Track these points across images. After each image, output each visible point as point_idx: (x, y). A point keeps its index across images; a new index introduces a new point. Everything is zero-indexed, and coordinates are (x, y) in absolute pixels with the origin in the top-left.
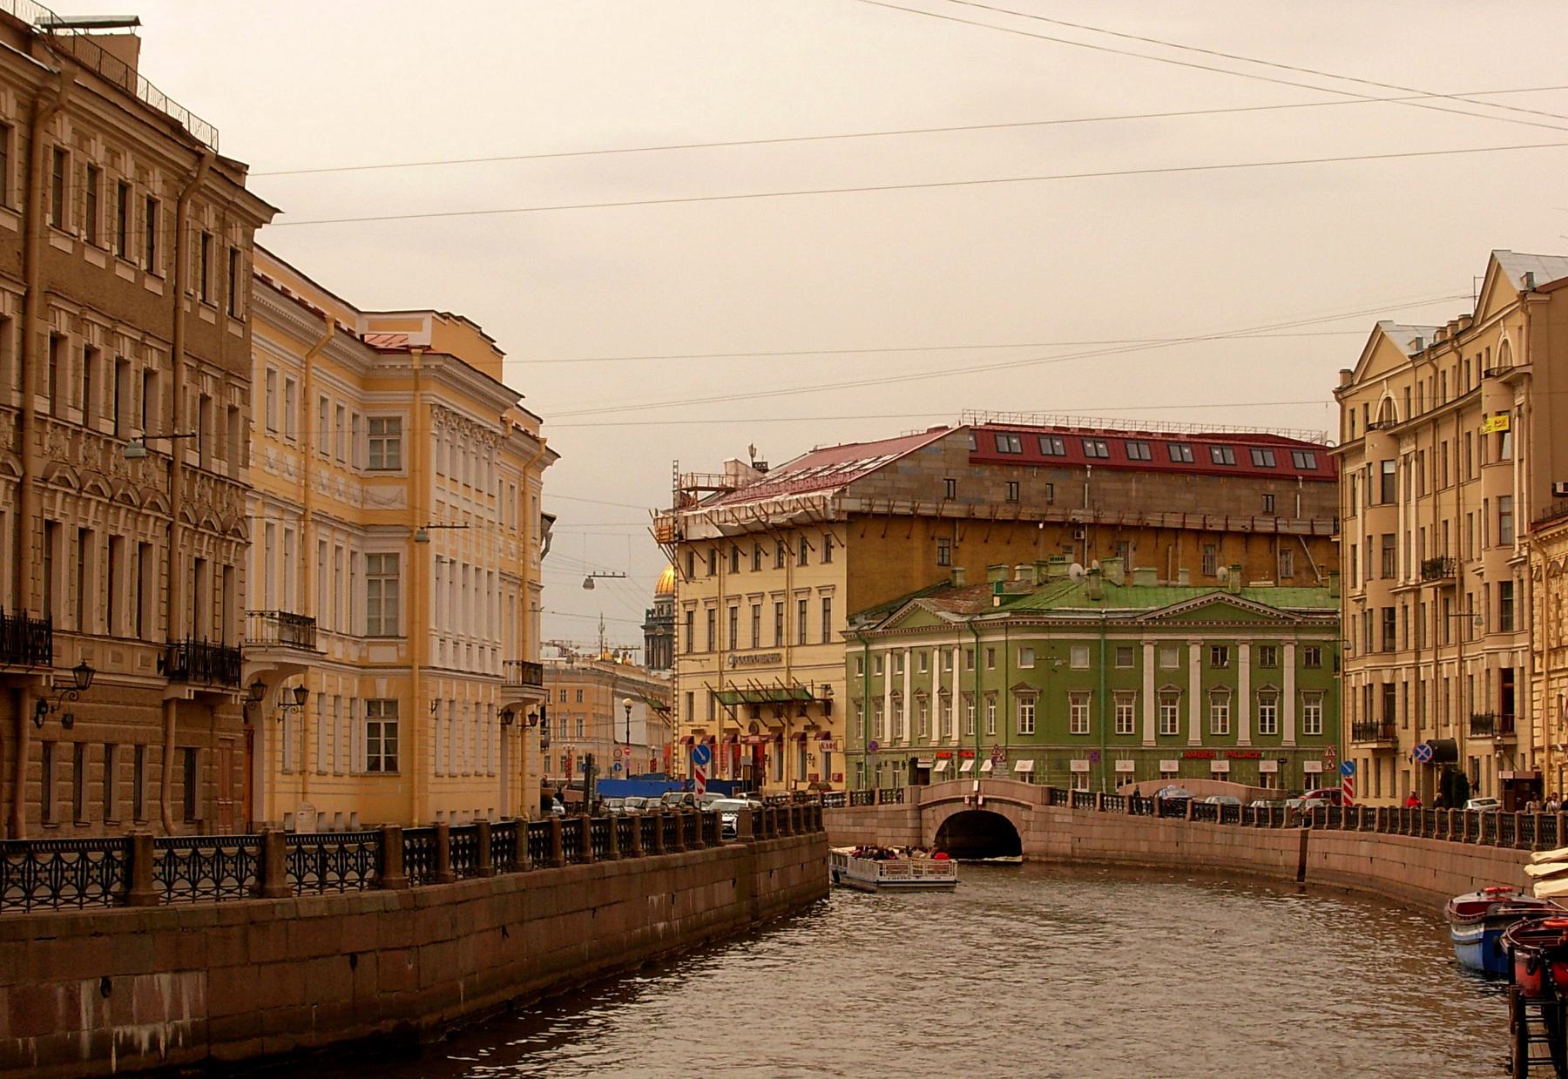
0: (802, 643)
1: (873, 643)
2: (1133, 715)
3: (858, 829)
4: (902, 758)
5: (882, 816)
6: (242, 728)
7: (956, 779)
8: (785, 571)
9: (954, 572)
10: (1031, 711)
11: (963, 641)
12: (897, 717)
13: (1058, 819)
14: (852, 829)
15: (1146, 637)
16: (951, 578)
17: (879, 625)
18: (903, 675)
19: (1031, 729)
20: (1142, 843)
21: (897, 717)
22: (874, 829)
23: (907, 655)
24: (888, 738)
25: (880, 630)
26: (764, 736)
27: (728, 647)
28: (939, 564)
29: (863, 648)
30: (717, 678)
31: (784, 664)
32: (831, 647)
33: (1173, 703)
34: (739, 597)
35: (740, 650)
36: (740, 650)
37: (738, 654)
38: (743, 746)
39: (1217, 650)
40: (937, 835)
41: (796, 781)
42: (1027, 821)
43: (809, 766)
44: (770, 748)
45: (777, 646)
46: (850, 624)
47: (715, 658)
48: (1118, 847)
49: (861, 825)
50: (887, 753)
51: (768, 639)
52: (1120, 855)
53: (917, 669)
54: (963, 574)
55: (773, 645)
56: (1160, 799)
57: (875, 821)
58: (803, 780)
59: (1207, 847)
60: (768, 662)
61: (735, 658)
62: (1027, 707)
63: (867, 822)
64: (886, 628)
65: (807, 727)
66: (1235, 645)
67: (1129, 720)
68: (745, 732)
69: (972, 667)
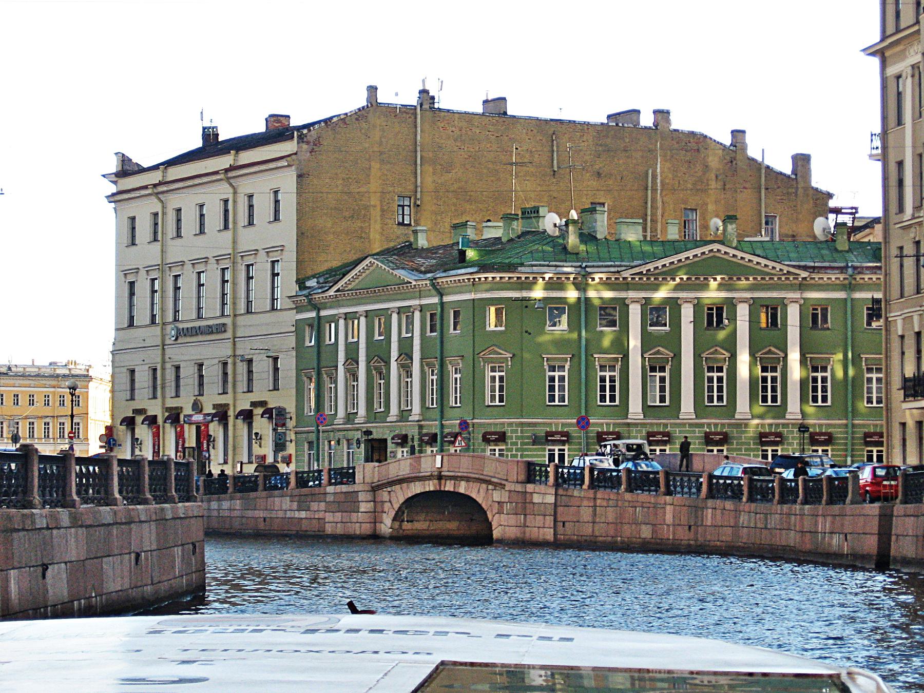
0: (249, 312)
1: (325, 308)
2: (617, 384)
3: (303, 514)
4: (358, 435)
5: (330, 498)
6: (228, 471)
7: (417, 455)
8: (159, 243)
9: (415, 232)
10: (501, 378)
11: (425, 301)
12: (351, 391)
13: (537, 499)
14: (297, 515)
15: (632, 294)
16: (412, 240)
17: (331, 287)
18: (412, 337)
19: (501, 400)
20: (643, 527)
21: (351, 391)
22: (321, 515)
23: (417, 315)
24: (341, 413)
25: (332, 293)
26: (208, 415)
27: (171, 319)
28: (399, 224)
29: (313, 314)
30: (160, 352)
31: (229, 334)
32: (278, 313)
33: (662, 369)
34: (183, 264)
35: (206, 319)
36: (206, 319)
37: (181, 326)
38: (186, 426)
39: (712, 309)
40: (394, 519)
41: (242, 463)
42: (499, 503)
43: (255, 446)
44: (215, 429)
45: (223, 315)
46: (300, 289)
47: (157, 330)
48: (612, 533)
49: (308, 509)
50: (340, 430)
51: (211, 308)
52: (616, 542)
53: (426, 333)
54: (425, 235)
55: (218, 314)
56: (711, 477)
57: (323, 504)
58: (250, 462)
59: (729, 531)
60: (212, 333)
61: (178, 329)
62: (497, 374)
63: (314, 506)
64: (338, 290)
65: (254, 404)
66: (783, 303)
67: (613, 388)
68: (188, 410)
69: (435, 331)
